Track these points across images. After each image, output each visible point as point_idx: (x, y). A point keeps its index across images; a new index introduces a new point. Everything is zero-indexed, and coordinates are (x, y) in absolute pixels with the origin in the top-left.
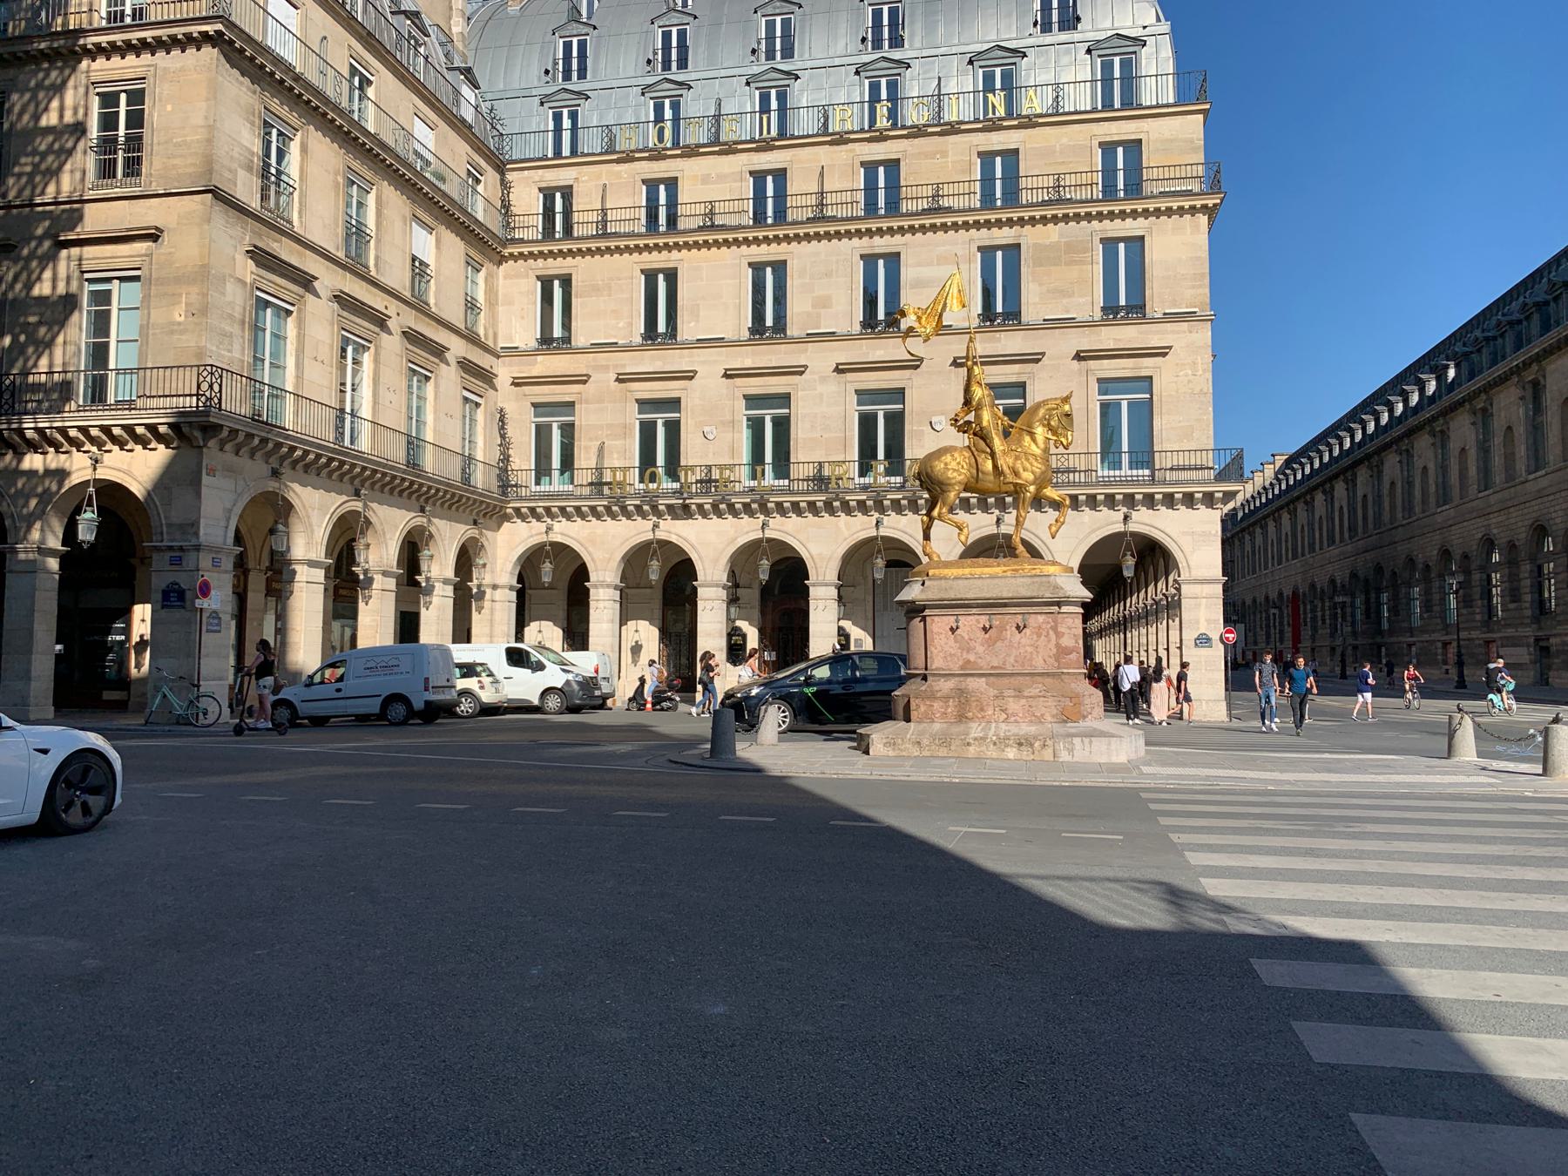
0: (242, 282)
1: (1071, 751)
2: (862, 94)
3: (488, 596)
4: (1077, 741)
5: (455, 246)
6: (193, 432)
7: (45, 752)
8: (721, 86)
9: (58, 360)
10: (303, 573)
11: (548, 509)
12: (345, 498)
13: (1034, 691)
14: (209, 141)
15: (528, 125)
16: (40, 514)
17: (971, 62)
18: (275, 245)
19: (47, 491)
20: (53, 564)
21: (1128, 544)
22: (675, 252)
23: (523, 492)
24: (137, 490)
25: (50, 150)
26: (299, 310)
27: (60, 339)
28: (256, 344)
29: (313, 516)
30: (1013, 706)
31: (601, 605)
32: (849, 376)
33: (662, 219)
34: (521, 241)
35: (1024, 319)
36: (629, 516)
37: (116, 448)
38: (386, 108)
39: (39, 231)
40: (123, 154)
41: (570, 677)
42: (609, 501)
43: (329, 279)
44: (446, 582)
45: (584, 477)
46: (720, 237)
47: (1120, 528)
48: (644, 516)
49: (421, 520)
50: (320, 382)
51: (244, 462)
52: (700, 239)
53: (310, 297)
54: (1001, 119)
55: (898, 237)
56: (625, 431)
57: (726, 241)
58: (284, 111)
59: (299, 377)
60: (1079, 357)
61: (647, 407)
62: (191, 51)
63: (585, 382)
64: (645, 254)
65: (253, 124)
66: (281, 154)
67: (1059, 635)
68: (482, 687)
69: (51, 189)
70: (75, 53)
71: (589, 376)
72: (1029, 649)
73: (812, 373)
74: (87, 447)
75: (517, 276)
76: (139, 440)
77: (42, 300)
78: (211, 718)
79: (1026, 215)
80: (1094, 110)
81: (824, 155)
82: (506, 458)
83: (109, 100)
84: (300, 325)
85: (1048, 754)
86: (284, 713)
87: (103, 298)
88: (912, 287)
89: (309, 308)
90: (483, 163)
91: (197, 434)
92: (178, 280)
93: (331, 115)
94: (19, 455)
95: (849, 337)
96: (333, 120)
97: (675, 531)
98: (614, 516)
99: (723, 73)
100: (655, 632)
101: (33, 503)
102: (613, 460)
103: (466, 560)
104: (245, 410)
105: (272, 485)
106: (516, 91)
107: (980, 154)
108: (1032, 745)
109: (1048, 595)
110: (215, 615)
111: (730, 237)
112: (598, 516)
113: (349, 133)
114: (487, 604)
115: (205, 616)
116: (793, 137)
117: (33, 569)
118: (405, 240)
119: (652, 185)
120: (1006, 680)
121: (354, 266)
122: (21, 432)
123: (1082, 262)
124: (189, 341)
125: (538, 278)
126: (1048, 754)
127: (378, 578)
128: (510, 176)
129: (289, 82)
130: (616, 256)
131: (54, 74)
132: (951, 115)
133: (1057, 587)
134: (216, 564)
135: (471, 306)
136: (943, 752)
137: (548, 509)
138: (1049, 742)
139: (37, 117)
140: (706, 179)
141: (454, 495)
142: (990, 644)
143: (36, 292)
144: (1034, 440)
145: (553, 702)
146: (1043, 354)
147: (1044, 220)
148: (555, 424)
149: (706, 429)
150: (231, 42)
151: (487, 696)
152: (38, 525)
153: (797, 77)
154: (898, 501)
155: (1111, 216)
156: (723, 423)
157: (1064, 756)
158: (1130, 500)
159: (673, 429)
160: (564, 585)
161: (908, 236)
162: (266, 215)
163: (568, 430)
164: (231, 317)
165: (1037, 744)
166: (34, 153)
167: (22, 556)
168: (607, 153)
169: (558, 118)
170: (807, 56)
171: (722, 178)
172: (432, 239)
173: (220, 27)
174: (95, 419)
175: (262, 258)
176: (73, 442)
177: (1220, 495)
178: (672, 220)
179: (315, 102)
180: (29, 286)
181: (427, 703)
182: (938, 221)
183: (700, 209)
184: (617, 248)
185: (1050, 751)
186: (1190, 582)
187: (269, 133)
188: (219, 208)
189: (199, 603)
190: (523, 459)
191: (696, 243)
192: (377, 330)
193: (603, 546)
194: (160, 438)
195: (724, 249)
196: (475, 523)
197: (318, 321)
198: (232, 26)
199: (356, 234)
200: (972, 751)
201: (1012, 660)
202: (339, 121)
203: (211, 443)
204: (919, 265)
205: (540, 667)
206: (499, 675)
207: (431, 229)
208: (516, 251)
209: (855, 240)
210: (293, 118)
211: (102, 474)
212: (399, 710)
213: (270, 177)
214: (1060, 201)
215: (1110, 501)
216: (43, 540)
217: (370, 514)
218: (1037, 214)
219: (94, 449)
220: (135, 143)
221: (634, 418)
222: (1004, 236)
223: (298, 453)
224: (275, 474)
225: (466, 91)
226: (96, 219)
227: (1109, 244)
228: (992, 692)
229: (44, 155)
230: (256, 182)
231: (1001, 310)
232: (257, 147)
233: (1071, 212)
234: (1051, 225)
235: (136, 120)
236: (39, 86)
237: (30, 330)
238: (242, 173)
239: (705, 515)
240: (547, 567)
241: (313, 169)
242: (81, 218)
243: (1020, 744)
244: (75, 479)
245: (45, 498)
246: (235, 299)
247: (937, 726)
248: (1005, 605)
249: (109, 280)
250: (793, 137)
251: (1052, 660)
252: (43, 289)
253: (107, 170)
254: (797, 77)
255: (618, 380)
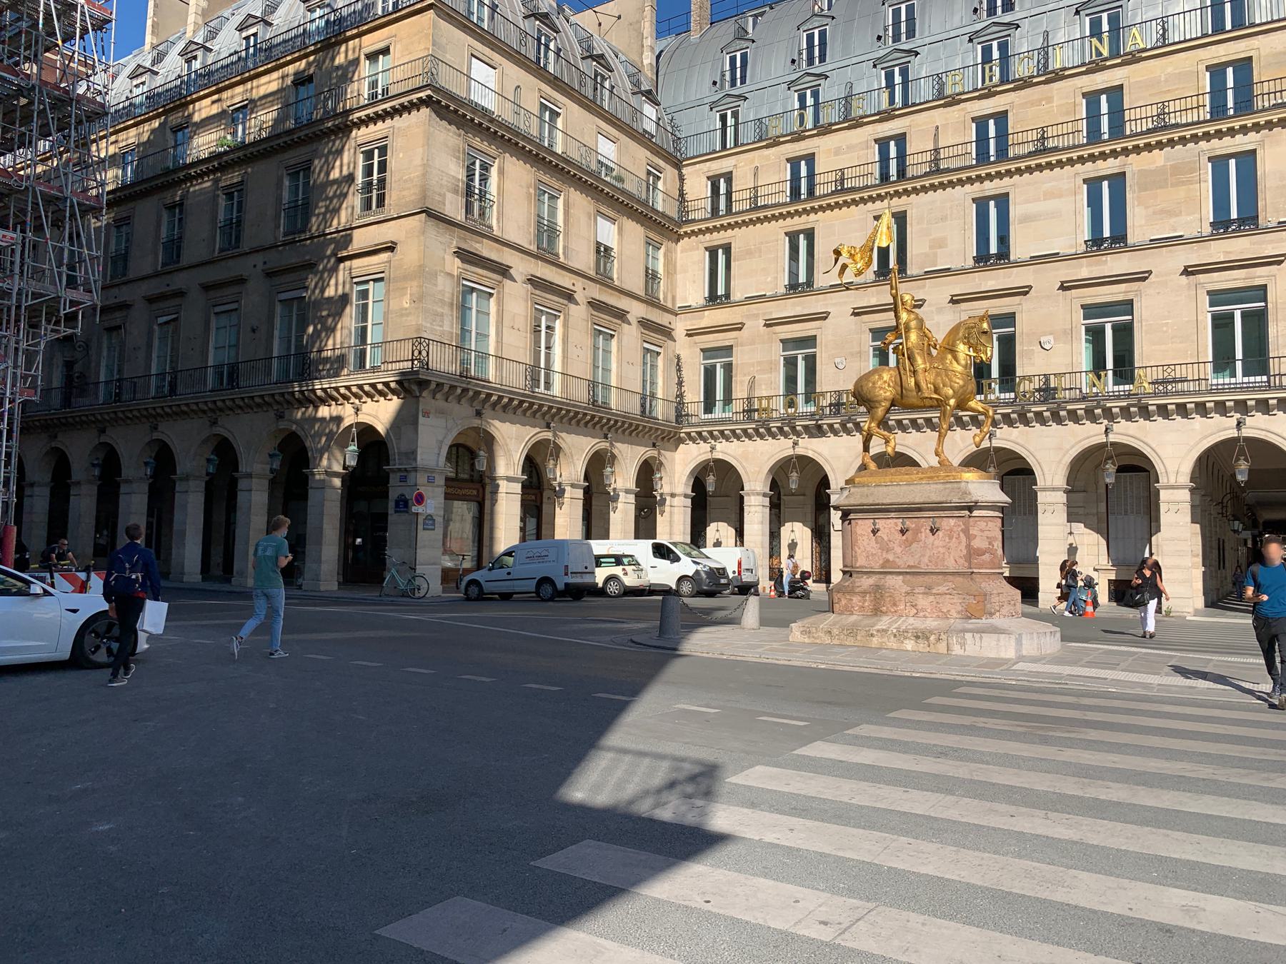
0: (450, 275)
1: (963, 645)
2: (975, 58)
3: (668, 503)
4: (968, 636)
5: (635, 230)
6: (412, 385)
7: (75, 611)
8: (855, 72)
9: (338, 341)
10: (504, 486)
11: (711, 433)
12: (538, 430)
13: (942, 589)
14: (424, 175)
15: (701, 125)
16: (327, 448)
17: (1077, 12)
18: (478, 246)
19: (331, 430)
20: (337, 482)
21: (1242, 449)
22: (812, 215)
23: (694, 420)
24: (381, 429)
25: (335, 196)
26: (498, 293)
27: (339, 326)
28: (463, 320)
29: (511, 445)
30: (923, 602)
31: (753, 509)
32: (964, 306)
33: (804, 190)
34: (694, 221)
35: (1130, 241)
36: (774, 436)
37: (382, 399)
38: (575, 132)
39: (329, 252)
40: (375, 194)
41: (699, 568)
42: (758, 424)
43: (521, 267)
44: (627, 491)
45: (738, 406)
46: (849, 198)
47: (1233, 433)
48: (786, 435)
49: (604, 445)
50: (518, 345)
51: (453, 406)
52: (832, 202)
53: (507, 282)
54: (1106, 59)
55: (1006, 179)
56: (771, 367)
57: (821, 207)
58: (484, 146)
59: (499, 341)
60: (1187, 272)
61: (790, 345)
62: (414, 113)
63: (740, 329)
64: (789, 219)
65: (458, 158)
66: (484, 179)
67: (969, 537)
68: (626, 574)
69: (335, 222)
70: (347, 126)
71: (743, 324)
72: (942, 550)
73: (930, 305)
74: (353, 400)
75: (692, 249)
76: (381, 393)
77: (330, 299)
78: (422, 593)
79: (1130, 145)
80: (1205, 36)
81: (939, 116)
82: (681, 395)
83: (369, 155)
84: (500, 303)
85: (942, 648)
86: (474, 591)
87: (364, 295)
88: (1021, 222)
89: (506, 290)
90: (661, 163)
91: (415, 387)
92: (406, 278)
93: (521, 143)
94: (316, 408)
95: (963, 271)
96: (524, 147)
97: (810, 447)
98: (762, 437)
99: (855, 60)
100: (807, 533)
101: (324, 439)
102: (762, 391)
103: (647, 473)
104: (454, 368)
105: (476, 422)
106: (691, 101)
107: (1084, 95)
108: (928, 639)
109: (956, 500)
110: (430, 518)
111: (857, 197)
112: (750, 437)
113: (537, 155)
114: (667, 509)
115: (421, 520)
116: (914, 105)
117: (323, 486)
118: (585, 228)
119: (794, 162)
120: (920, 579)
121: (545, 253)
122: (314, 391)
123: (1190, 182)
124: (412, 321)
125: (706, 249)
126: (942, 648)
127: (568, 489)
128: (684, 171)
129: (486, 124)
130: (766, 224)
131: (338, 142)
132: (1056, 63)
133: (966, 493)
134: (431, 480)
135: (651, 276)
136: (850, 641)
137: (711, 433)
138: (943, 636)
139: (328, 174)
140: (838, 151)
141: (631, 424)
142: (908, 544)
143: (326, 294)
144: (956, 358)
145: (686, 588)
146: (1150, 272)
147: (1149, 147)
148: (719, 364)
149: (837, 360)
150: (439, 102)
151: (630, 580)
152: (326, 456)
153: (917, 54)
154: (1008, 415)
155: (1219, 134)
156: (852, 354)
157: (957, 650)
158: (1242, 407)
159: (811, 362)
160: (811, 492)
161: (1016, 177)
162: (469, 224)
163: (728, 368)
164: (442, 301)
165: (932, 638)
166: (327, 198)
167: (317, 477)
168: (759, 141)
169: (723, 118)
170: (927, 34)
171: (851, 148)
172: (614, 228)
173: (429, 92)
174: (365, 379)
175: (464, 255)
176: (345, 397)
177: (1275, 401)
178: (811, 192)
179: (508, 136)
180: (323, 291)
181: (566, 585)
182: (1043, 161)
183: (832, 177)
184: (766, 217)
185: (944, 644)
186: (1044, 490)
187: (474, 164)
188: (431, 222)
189: (414, 509)
190: (694, 394)
191: (829, 205)
192: (565, 302)
193: (754, 460)
194: (394, 392)
195: (853, 207)
196: (654, 445)
197: (515, 300)
198: (437, 90)
199: (546, 232)
200: (875, 642)
201: (926, 560)
202: (528, 147)
203: (425, 394)
204: (1027, 201)
205: (677, 559)
206: (643, 565)
207: (613, 221)
208: (688, 229)
209: (968, 187)
210: (492, 150)
211: (362, 418)
212: (548, 590)
213: (473, 194)
214: (1166, 127)
215: (1221, 408)
216: (330, 466)
217: (560, 442)
218: (1141, 143)
219: (357, 401)
220: (382, 182)
221: (778, 354)
222: (1109, 166)
223: (494, 398)
224: (479, 414)
225: (649, 110)
226: (361, 239)
227: (1219, 163)
228: (906, 588)
229: (331, 199)
230: (461, 201)
231: (1109, 237)
232: (461, 175)
233: (1176, 136)
234: (1156, 152)
235: (383, 167)
236: (330, 152)
237: (323, 320)
238: (449, 196)
239: (836, 433)
240: (794, 476)
241: (508, 185)
242: (351, 241)
243: (917, 637)
244: (346, 423)
245: (330, 436)
246: (445, 288)
247: (853, 618)
248: (920, 510)
249: (367, 282)
250: (914, 105)
251: (962, 561)
252: (330, 292)
253: (367, 205)
254: (917, 54)
255: (766, 325)
